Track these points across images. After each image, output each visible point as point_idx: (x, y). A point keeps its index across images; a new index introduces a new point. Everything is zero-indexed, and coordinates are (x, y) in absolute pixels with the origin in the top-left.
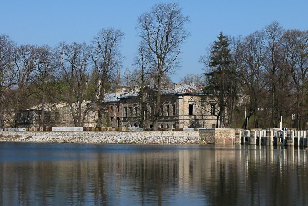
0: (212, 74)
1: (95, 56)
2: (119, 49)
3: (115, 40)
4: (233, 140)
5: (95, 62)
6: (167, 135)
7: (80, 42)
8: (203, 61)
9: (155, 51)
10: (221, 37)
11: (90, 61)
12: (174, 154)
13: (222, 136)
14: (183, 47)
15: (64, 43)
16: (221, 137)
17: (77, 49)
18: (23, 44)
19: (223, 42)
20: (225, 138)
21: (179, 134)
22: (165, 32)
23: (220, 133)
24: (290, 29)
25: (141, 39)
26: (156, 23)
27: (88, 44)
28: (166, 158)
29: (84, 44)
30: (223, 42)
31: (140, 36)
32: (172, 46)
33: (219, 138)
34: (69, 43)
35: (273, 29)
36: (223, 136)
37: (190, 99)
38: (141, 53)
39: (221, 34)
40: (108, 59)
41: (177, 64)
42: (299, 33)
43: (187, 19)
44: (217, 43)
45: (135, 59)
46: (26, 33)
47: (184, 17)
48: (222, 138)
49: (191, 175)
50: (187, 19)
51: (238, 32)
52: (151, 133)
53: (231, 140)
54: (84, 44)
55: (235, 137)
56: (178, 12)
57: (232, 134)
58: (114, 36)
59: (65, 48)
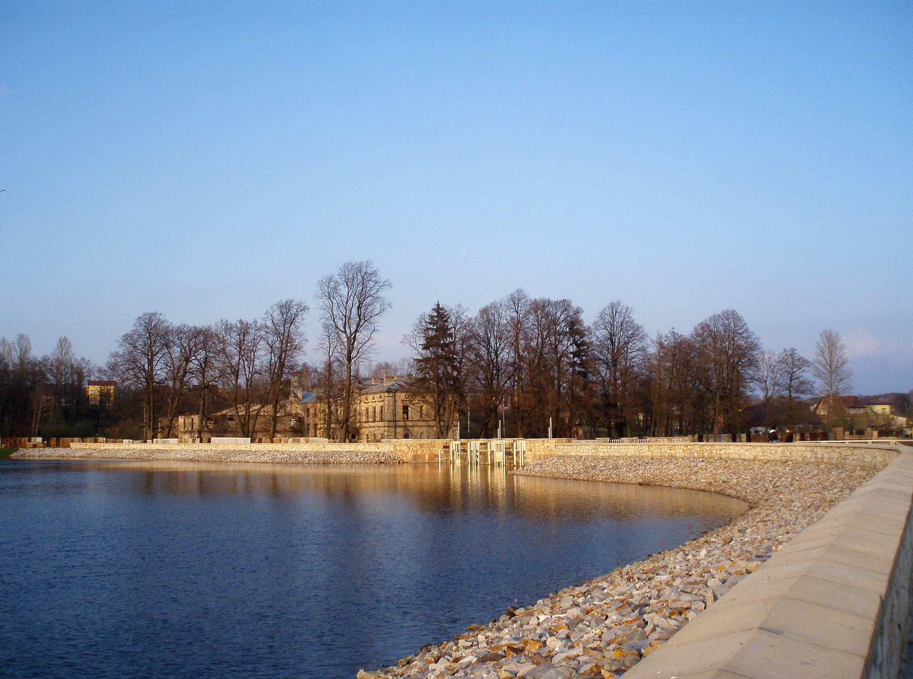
0: (426, 360)
1: (271, 338)
2: (301, 329)
7: (248, 319)
9: (745, 506)
10: (438, 309)
12: (395, 475)
17: (244, 330)
19: (440, 318)
24: (538, 298)
25: (323, 312)
26: (344, 290)
27: (260, 322)
30: (440, 318)
34: (233, 320)
35: (516, 300)
39: (438, 305)
40: (286, 344)
42: (549, 302)
44: (432, 317)
49: (136, 414)
50: (388, 284)
51: (467, 304)
54: (255, 322)
56: (374, 273)
58: (294, 311)
59: (229, 328)
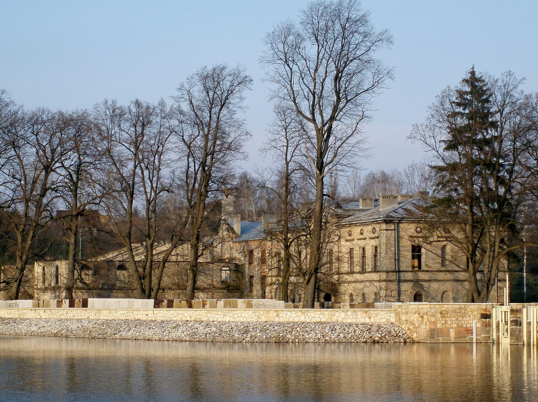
1: (188, 131)
3: (231, 92)
4: (474, 331)
5: (189, 147)
6: (318, 320)
7: (151, 100)
8: (419, 137)
10: (473, 80)
11: (173, 142)
13: (446, 322)
14: (375, 103)
15: (114, 102)
16: (443, 324)
17: (143, 118)
18: (34, 109)
20: (455, 325)
21: (347, 317)
22: (335, 67)
23: (441, 313)
26: (310, 49)
27: (170, 104)
28: (392, 352)
29: (162, 104)
31: (273, 80)
32: (347, 103)
33: (439, 326)
34: (125, 101)
36: (449, 322)
37: (413, 231)
38: (283, 123)
39: (473, 73)
41: (361, 145)
43: (385, 38)
44: (461, 94)
45: (270, 135)
46: (52, 86)
47: (378, 32)
48: (448, 326)
50: (385, 38)
52: (280, 315)
53: (469, 331)
55: (479, 325)
57: (472, 317)
59: (117, 115)
